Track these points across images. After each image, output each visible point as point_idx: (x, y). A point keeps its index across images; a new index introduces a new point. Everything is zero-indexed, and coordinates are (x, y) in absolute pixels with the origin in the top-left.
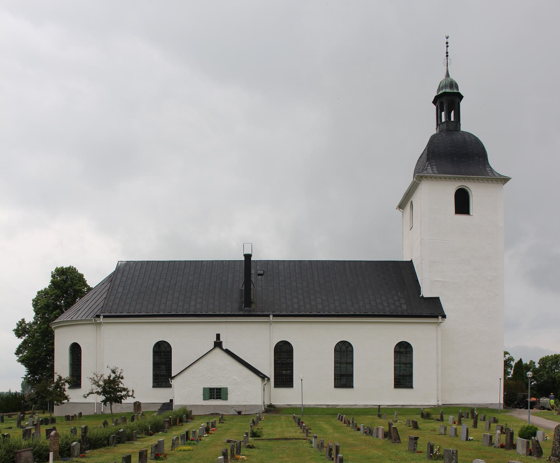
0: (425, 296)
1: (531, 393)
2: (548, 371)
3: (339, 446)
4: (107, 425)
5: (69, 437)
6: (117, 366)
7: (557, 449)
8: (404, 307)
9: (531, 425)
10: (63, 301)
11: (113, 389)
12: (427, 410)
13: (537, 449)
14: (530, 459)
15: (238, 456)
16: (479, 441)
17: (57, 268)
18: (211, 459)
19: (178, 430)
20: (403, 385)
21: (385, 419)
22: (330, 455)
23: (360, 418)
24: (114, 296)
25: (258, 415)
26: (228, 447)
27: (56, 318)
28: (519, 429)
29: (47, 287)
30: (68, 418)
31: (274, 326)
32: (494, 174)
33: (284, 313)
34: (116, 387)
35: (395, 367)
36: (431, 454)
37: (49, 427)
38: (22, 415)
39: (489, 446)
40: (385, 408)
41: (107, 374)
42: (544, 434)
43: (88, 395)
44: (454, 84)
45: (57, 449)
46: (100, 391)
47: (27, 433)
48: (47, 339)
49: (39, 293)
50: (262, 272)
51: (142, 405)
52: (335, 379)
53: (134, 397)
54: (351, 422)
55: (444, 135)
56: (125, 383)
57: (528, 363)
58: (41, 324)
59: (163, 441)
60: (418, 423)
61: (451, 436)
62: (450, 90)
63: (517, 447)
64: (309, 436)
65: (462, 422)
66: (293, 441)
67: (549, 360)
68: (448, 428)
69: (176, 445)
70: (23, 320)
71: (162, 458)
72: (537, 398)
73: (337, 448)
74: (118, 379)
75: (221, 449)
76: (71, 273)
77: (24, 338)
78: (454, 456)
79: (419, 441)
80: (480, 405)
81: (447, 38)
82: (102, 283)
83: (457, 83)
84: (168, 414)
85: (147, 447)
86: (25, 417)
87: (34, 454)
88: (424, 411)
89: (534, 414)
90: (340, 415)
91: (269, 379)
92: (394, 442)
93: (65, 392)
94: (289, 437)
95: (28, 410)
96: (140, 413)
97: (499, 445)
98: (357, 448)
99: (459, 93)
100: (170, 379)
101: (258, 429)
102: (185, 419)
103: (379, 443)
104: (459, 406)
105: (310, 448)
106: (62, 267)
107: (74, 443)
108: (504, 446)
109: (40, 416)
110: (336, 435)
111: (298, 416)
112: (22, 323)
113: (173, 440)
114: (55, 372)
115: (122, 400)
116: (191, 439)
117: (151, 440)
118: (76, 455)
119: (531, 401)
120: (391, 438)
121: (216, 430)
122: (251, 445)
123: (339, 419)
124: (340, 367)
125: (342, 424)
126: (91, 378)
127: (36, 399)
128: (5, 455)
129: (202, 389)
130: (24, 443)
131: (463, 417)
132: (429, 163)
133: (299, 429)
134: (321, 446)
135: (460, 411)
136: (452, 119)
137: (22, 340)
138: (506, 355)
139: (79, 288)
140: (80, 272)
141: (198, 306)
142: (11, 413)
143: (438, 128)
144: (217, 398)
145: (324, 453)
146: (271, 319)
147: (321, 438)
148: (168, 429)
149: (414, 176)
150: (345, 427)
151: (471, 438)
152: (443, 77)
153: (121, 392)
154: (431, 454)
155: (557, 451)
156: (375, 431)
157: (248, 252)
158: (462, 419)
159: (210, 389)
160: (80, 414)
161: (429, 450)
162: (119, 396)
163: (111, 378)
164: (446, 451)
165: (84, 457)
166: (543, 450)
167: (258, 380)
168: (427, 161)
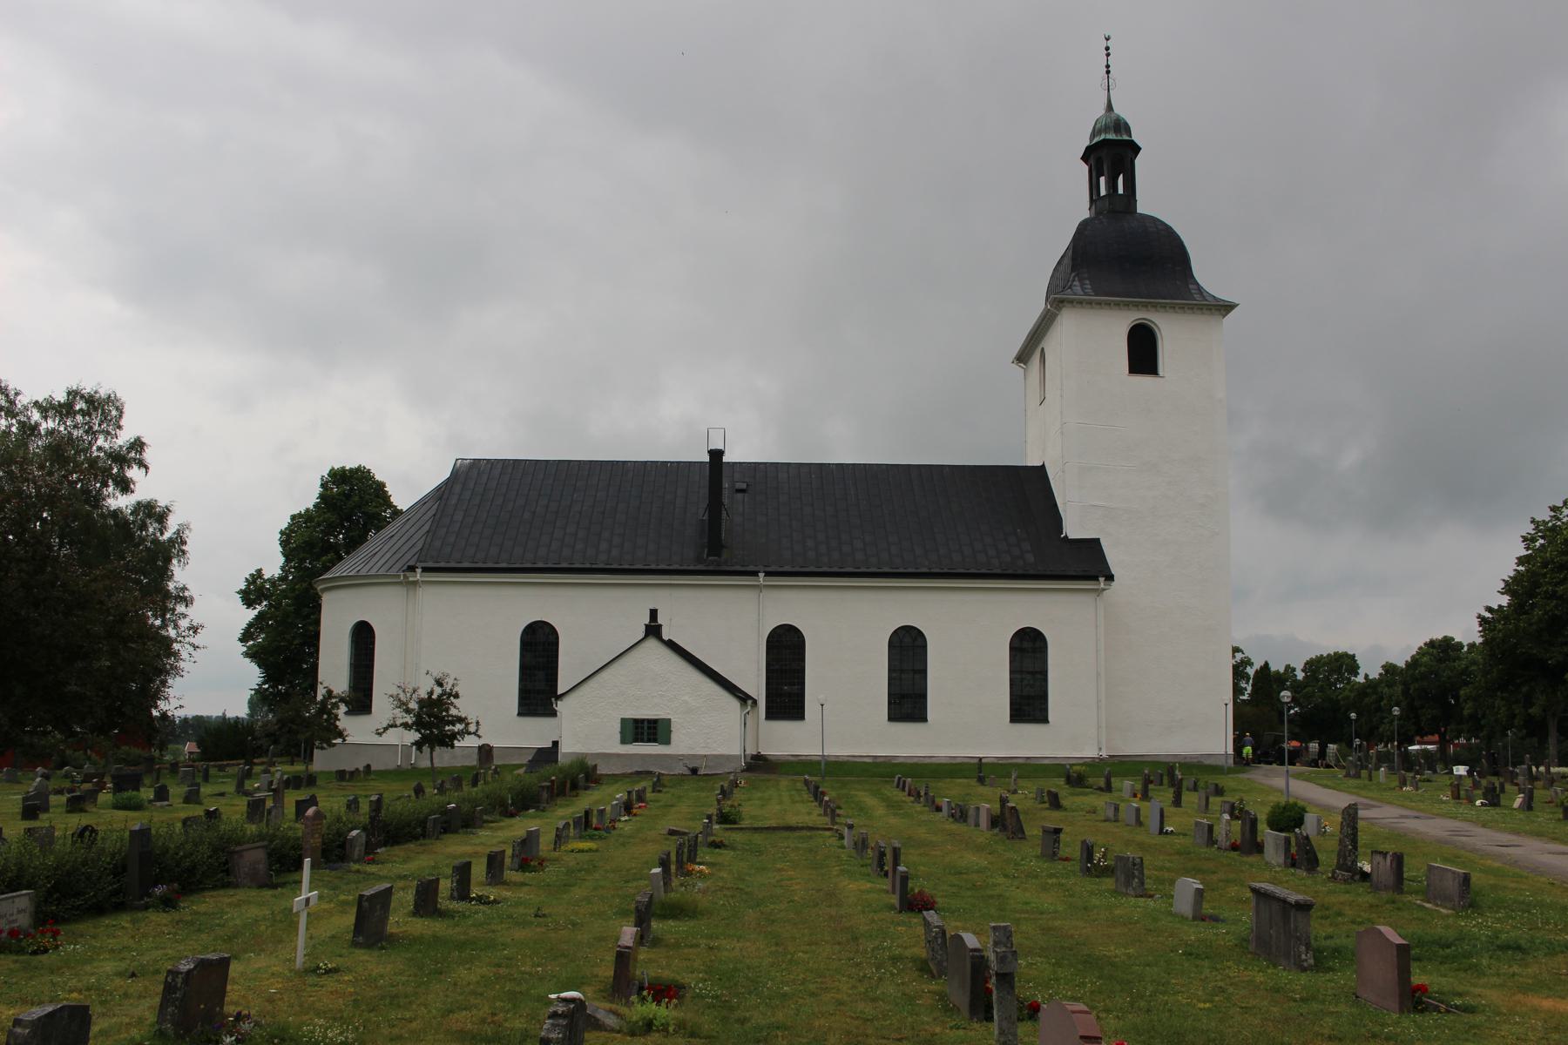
0: (1071, 536)
1: (1290, 732)
2: (1322, 686)
3: (899, 849)
4: (423, 796)
5: (344, 819)
6: (446, 671)
7: (1347, 854)
8: (1030, 558)
9: (1291, 800)
10: (341, 536)
11: (436, 717)
12: (1078, 768)
13: (1307, 854)
14: (1293, 874)
15: (691, 867)
16: (1185, 835)
17: (333, 469)
18: (635, 871)
19: (567, 805)
20: (1029, 716)
21: (991, 786)
22: (881, 865)
23: (940, 784)
24: (445, 529)
25: (732, 778)
26: (671, 846)
27: (326, 569)
28: (1267, 809)
29: (312, 507)
30: (341, 775)
31: (766, 594)
32: (1204, 297)
33: (787, 568)
34: (444, 714)
35: (1011, 680)
36: (1089, 865)
37: (302, 795)
38: (247, 767)
39: (1207, 846)
40: (993, 764)
41: (425, 687)
42: (1319, 821)
43: (386, 729)
44: (1122, 125)
45: (318, 844)
46: (410, 722)
47: (256, 809)
48: (306, 611)
49: (293, 517)
51: (495, 752)
52: (890, 703)
53: (479, 737)
54: (922, 793)
55: (1104, 220)
56: (461, 707)
57: (1282, 670)
58: (295, 580)
59: (538, 830)
60: (1059, 796)
61: (1128, 825)
62: (1114, 135)
63: (1265, 850)
64: (837, 823)
65: (1150, 794)
66: (805, 833)
67: (1325, 664)
68: (1122, 806)
69: (563, 840)
70: (259, 571)
71: (535, 866)
72: (1301, 742)
73: (896, 853)
74: (448, 698)
75: (654, 850)
76: (360, 479)
77: (259, 608)
78: (1137, 869)
79: (1062, 836)
80: (1185, 757)
81: (1107, 39)
82: (422, 502)
83: (1128, 122)
84: (548, 772)
85: (504, 843)
86: (254, 771)
87: (270, 855)
88: (1071, 771)
89: (1298, 776)
90: (899, 778)
91: (755, 702)
92: (1013, 838)
93: (338, 723)
94: (795, 825)
95: (260, 756)
96: (490, 768)
97: (1228, 843)
98: (935, 850)
99: (1133, 141)
100: (553, 699)
101: (732, 806)
102: (582, 783)
103: (980, 840)
105: (841, 850)
106: (343, 467)
107: (354, 833)
108: (1237, 846)
109: (282, 770)
110: (893, 821)
111: (814, 778)
112: (257, 579)
113: (557, 829)
114: (319, 680)
115: (456, 742)
116: (594, 826)
117: (511, 826)
118: (356, 857)
119: (1291, 749)
120: (1004, 828)
121: (645, 807)
122: (717, 839)
123: (898, 787)
124: (901, 679)
125: (904, 796)
126: (392, 696)
127: (278, 733)
128: (210, 857)
129: (619, 721)
130: (252, 828)
131: (1151, 782)
132: (1077, 275)
133: (816, 806)
134: (861, 845)
135: (1146, 772)
136: (1121, 191)
137: (256, 612)
138: (1236, 654)
139: (375, 510)
140: (378, 477)
141: (615, 552)
142: (225, 763)
143: (1094, 207)
144: (649, 741)
145: (869, 861)
146: (761, 579)
147: (861, 826)
148: (548, 803)
149: (1047, 300)
150: (910, 804)
151: (1170, 829)
152: (1100, 111)
153: (454, 725)
154: (1089, 865)
155: (1349, 858)
156: (971, 812)
157: (717, 445)
158: (1151, 786)
159: (636, 721)
160: (368, 767)
161: (1085, 856)
162: (449, 733)
163: (435, 697)
164: (1119, 859)
165: (372, 861)
166: (1320, 856)
167: (734, 703)
168: (1072, 271)
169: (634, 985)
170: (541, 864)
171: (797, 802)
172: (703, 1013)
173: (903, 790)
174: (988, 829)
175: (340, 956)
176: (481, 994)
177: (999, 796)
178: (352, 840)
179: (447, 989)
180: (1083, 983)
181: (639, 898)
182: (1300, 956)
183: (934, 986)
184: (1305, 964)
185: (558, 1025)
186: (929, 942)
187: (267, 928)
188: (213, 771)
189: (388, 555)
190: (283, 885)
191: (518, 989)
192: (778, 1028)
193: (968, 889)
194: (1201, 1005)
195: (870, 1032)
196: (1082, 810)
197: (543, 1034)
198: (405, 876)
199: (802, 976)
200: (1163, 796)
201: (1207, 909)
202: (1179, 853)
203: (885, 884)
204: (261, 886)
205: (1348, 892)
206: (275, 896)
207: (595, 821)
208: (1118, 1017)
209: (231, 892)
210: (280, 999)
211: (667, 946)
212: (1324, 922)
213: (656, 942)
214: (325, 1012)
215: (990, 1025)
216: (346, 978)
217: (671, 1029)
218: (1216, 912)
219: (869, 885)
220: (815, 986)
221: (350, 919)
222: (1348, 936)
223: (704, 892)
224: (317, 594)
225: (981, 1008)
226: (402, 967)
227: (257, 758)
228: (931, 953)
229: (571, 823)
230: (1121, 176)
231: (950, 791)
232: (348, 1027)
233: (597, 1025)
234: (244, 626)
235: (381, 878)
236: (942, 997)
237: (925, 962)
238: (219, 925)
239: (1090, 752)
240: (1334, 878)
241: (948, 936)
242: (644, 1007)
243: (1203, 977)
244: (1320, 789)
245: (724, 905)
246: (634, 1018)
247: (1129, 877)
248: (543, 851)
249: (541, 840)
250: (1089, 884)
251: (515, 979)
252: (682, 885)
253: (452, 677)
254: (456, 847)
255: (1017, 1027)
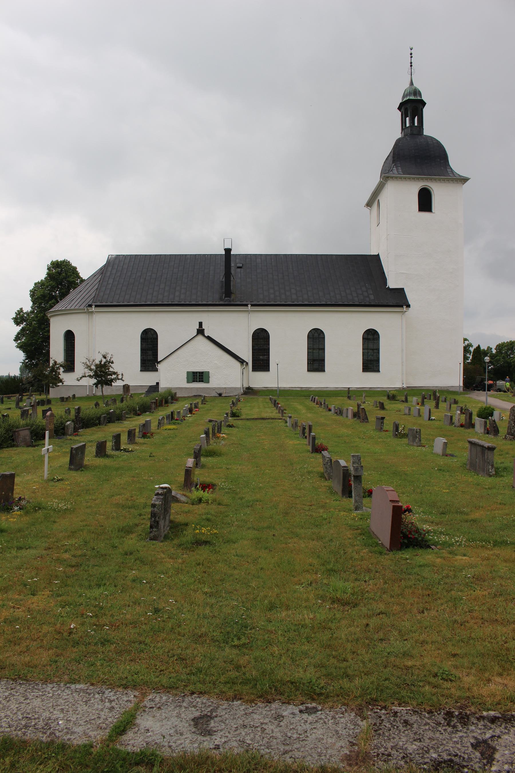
1: (489, 376)
2: (504, 356)
3: (312, 425)
6: (107, 352)
7: (512, 427)
8: (372, 297)
9: (488, 406)
11: (104, 372)
12: (393, 392)
13: (494, 428)
14: (487, 437)
15: (218, 435)
17: (53, 261)
18: (194, 437)
19: (163, 410)
20: (371, 369)
21: (354, 400)
22: (304, 433)
23: (331, 399)
25: (237, 397)
26: (210, 426)
27: (51, 307)
29: (44, 279)
30: (62, 399)
32: (454, 175)
35: (363, 353)
37: (45, 407)
38: (20, 397)
40: (355, 391)
41: (98, 359)
42: (500, 414)
43: (81, 378)
44: (417, 92)
46: (92, 375)
47: (24, 414)
48: (43, 326)
49: (35, 284)
50: (241, 265)
51: (131, 388)
52: (308, 363)
53: (123, 381)
54: (323, 404)
55: (408, 138)
56: (115, 368)
57: (486, 349)
63: (475, 427)
64: (284, 416)
66: (269, 421)
68: (412, 408)
69: (161, 425)
70: (21, 309)
71: (149, 436)
72: (493, 381)
73: (310, 427)
74: (109, 364)
75: (203, 428)
76: (65, 266)
77: (22, 326)
79: (385, 421)
80: (441, 387)
81: (411, 49)
82: (94, 275)
85: (135, 426)
87: (31, 433)
89: (491, 396)
90: (312, 397)
91: (247, 363)
93: (60, 376)
94: (265, 417)
96: (128, 395)
97: (459, 424)
99: (422, 100)
100: (156, 364)
102: (170, 400)
103: (348, 423)
104: (422, 388)
106: (57, 260)
107: (68, 423)
109: (36, 397)
110: (309, 415)
111: (274, 398)
113: (159, 420)
114: (51, 357)
115: (113, 383)
118: (70, 433)
120: (359, 417)
122: (231, 424)
123: (312, 400)
124: (313, 353)
128: (4, 434)
130: (22, 422)
131: (426, 398)
132: (395, 165)
134: (295, 425)
135: (423, 393)
136: (416, 124)
137: (21, 328)
138: (465, 342)
139: (73, 280)
140: (74, 265)
141: (182, 296)
142: (10, 395)
143: (403, 132)
144: (200, 381)
145: (298, 432)
148: (155, 410)
151: (433, 418)
152: (407, 85)
153: (112, 376)
156: (345, 411)
157: (228, 246)
158: (425, 400)
159: (194, 373)
160: (74, 395)
161: (395, 429)
163: (102, 363)
164: (410, 430)
165: (77, 435)
166: (500, 429)
167: (238, 364)
168: (393, 163)
169: (193, 484)
170: (152, 435)
171: (266, 408)
172: (224, 495)
173: (314, 402)
174: (352, 418)
175: (64, 474)
176: (126, 489)
177: (356, 404)
178: (67, 426)
179: (111, 487)
180: (392, 482)
181: (195, 447)
182: (489, 470)
183: (327, 483)
184: (491, 474)
185: (159, 498)
186: (324, 464)
187: (31, 463)
188: (5, 399)
189: (79, 300)
190: (38, 445)
191: (142, 486)
192: (257, 501)
193: (342, 443)
194: (445, 491)
195: (298, 502)
196: (394, 410)
197: (153, 502)
198: (92, 441)
199: (268, 480)
200: (430, 404)
201: (448, 452)
202: (437, 428)
203: (306, 441)
204: (28, 446)
205: (511, 444)
206: (34, 450)
207: (176, 417)
208: (408, 496)
209: (15, 448)
210: (38, 492)
211: (208, 468)
212: (500, 457)
213: (203, 466)
214: (57, 497)
215: (351, 499)
216: (67, 483)
217: (210, 502)
218: (453, 453)
219: (298, 442)
220: (273, 484)
221: (68, 459)
222: (511, 463)
223: (225, 445)
224: (48, 318)
225: (347, 492)
226: (91, 478)
227: (24, 393)
228: (325, 469)
229: (165, 417)
230: (417, 117)
231: (334, 403)
232: (68, 503)
233: (176, 500)
234: (16, 334)
235: (81, 442)
236: (330, 488)
237: (323, 474)
238: (10, 462)
239: (399, 385)
240: (505, 438)
241: (333, 461)
242: (198, 493)
243: (446, 479)
244: (501, 401)
245: (233, 451)
246: (194, 497)
247: (415, 437)
248: (153, 429)
249: (152, 425)
250: (396, 441)
251: (141, 482)
252: (214, 442)
253: (110, 354)
254: (114, 428)
255: (362, 499)
